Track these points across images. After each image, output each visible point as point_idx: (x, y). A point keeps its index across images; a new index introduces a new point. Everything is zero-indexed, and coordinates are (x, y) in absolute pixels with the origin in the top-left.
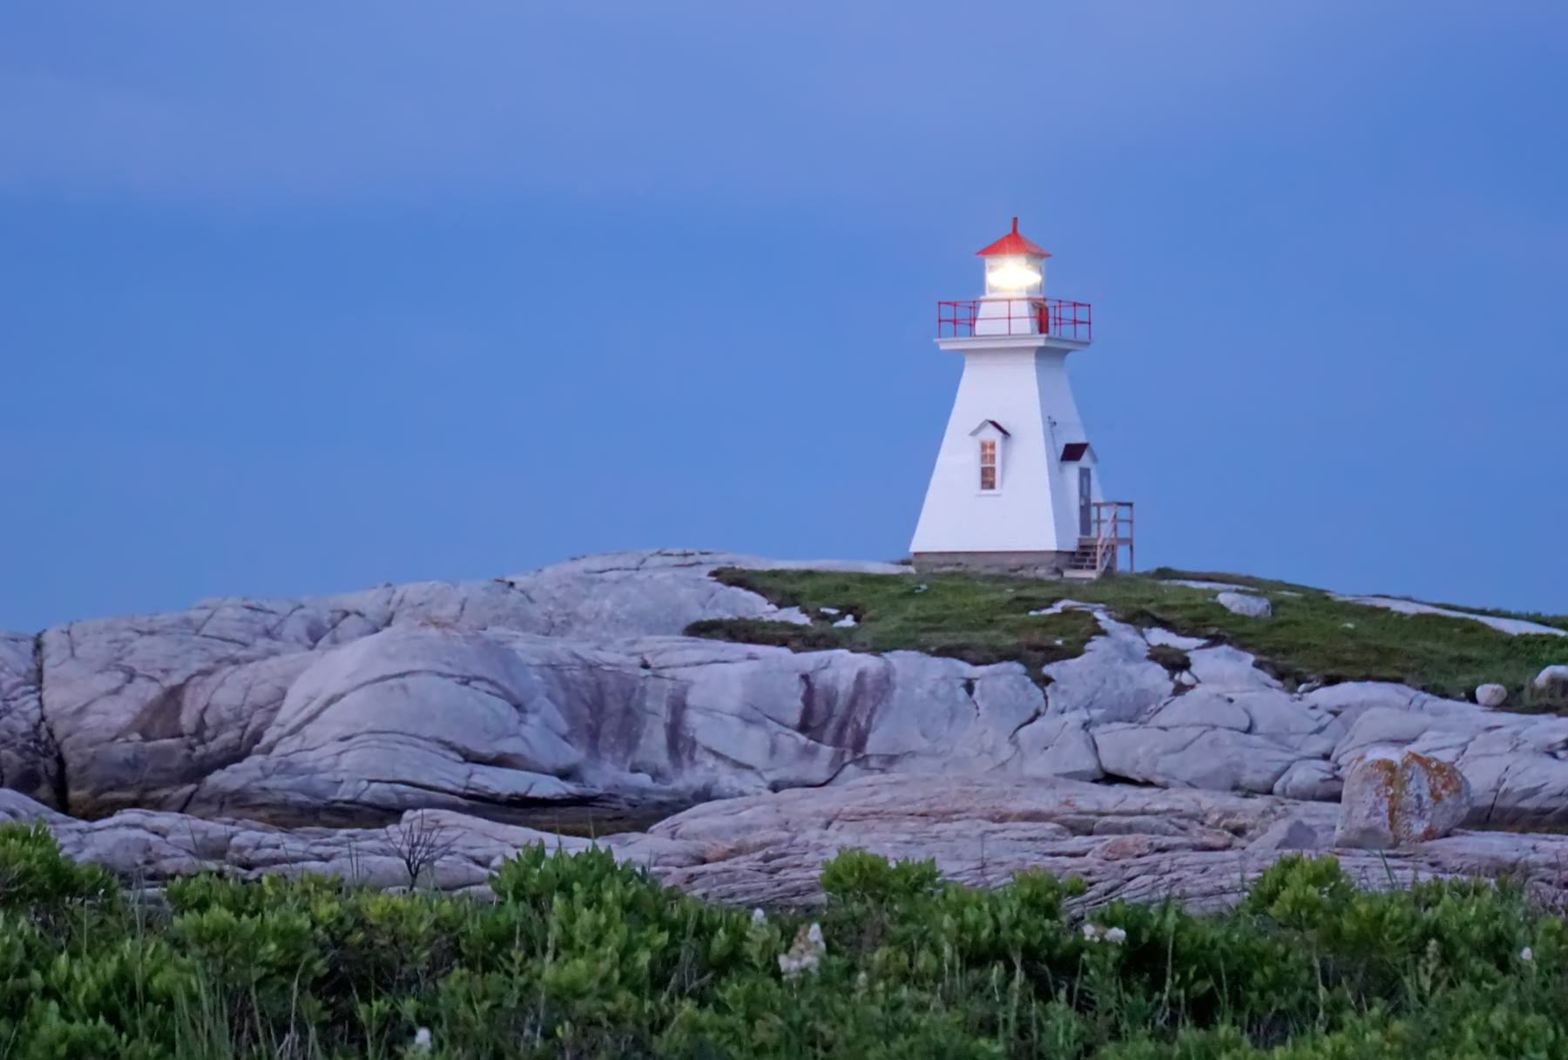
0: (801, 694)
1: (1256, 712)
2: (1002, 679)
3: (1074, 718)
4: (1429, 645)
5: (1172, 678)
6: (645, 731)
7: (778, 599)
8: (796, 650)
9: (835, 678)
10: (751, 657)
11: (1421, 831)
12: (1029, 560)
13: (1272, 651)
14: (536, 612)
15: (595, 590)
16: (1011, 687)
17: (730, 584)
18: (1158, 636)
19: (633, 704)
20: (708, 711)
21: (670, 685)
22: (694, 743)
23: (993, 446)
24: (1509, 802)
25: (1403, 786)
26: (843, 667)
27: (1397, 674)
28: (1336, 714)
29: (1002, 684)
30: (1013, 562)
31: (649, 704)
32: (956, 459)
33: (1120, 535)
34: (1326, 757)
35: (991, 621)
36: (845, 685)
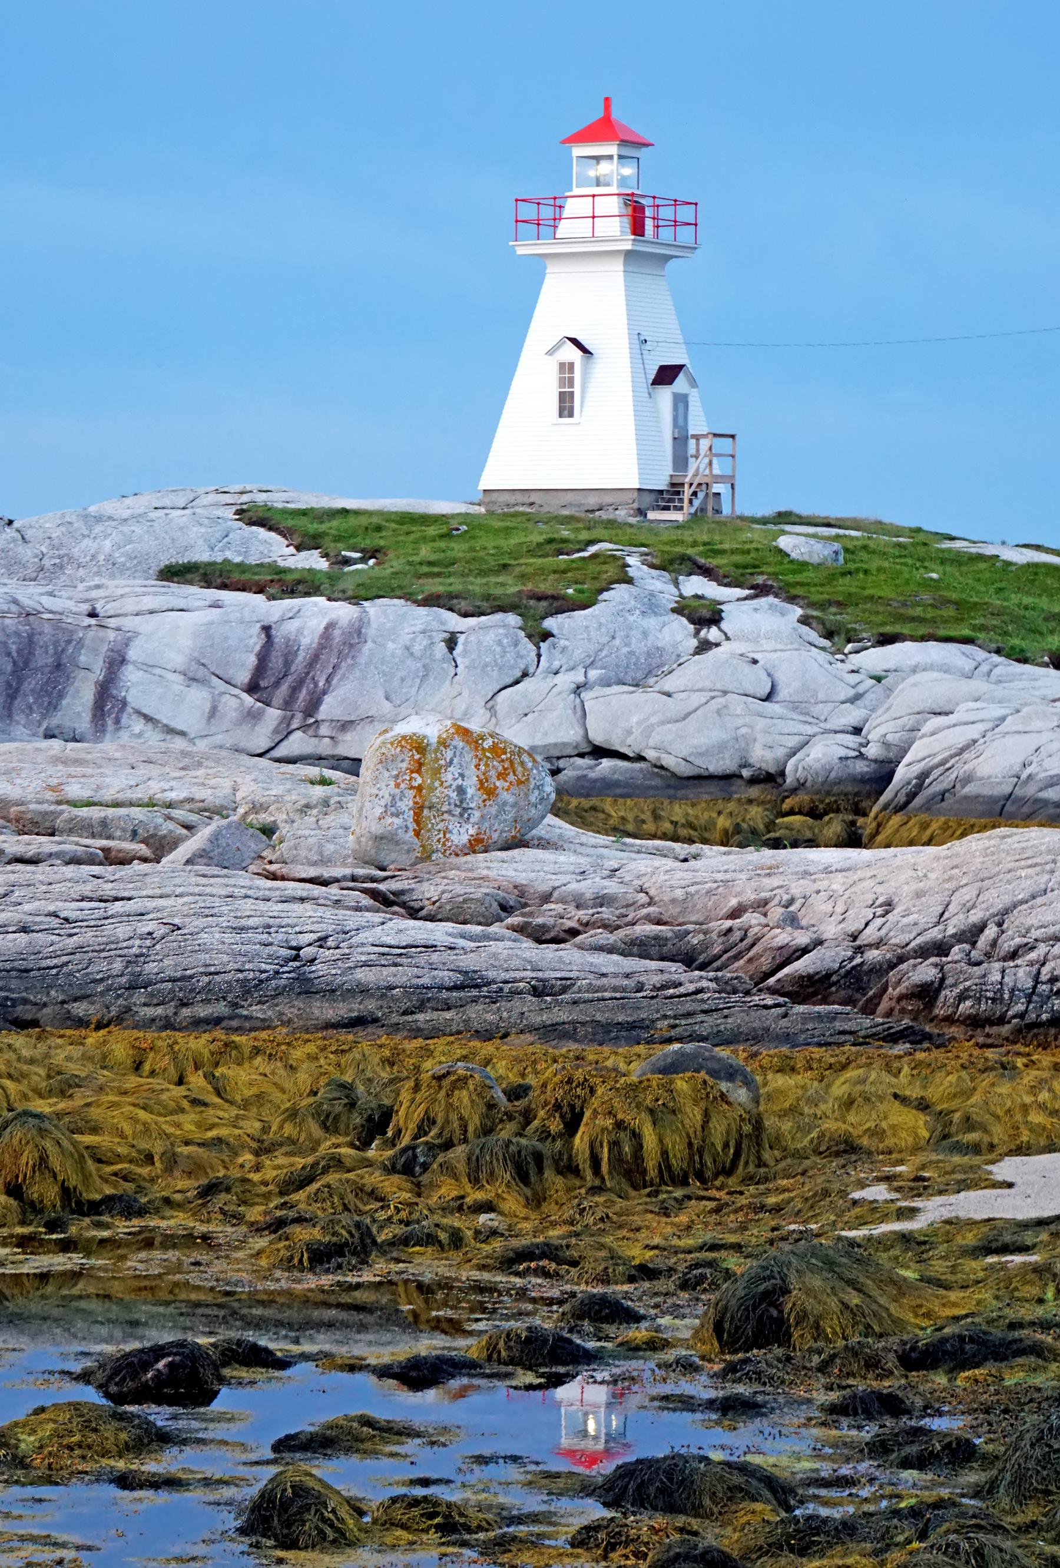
0: (258, 648)
1: (781, 677)
2: (493, 634)
3: (566, 680)
4: (1028, 600)
5: (697, 633)
6: (71, 690)
7: (297, 540)
8: (272, 598)
9: (300, 631)
10: (216, 605)
11: (465, 839)
12: (608, 499)
13: (822, 606)
14: (26, 553)
15: (98, 529)
16: (499, 643)
17: (251, 523)
18: (695, 585)
19: (64, 660)
20: (148, 667)
21: (111, 635)
22: (124, 703)
23: (571, 366)
24: (1030, 790)
25: (436, 772)
26: (311, 617)
27: (967, 632)
28: (878, 679)
29: (490, 638)
30: (592, 501)
31: (83, 659)
32: (534, 380)
33: (716, 471)
34: (857, 731)
35: (505, 566)
36: (309, 640)
